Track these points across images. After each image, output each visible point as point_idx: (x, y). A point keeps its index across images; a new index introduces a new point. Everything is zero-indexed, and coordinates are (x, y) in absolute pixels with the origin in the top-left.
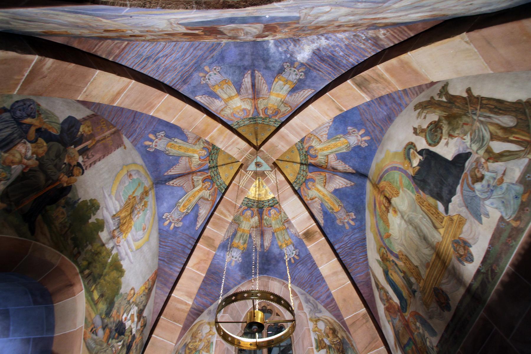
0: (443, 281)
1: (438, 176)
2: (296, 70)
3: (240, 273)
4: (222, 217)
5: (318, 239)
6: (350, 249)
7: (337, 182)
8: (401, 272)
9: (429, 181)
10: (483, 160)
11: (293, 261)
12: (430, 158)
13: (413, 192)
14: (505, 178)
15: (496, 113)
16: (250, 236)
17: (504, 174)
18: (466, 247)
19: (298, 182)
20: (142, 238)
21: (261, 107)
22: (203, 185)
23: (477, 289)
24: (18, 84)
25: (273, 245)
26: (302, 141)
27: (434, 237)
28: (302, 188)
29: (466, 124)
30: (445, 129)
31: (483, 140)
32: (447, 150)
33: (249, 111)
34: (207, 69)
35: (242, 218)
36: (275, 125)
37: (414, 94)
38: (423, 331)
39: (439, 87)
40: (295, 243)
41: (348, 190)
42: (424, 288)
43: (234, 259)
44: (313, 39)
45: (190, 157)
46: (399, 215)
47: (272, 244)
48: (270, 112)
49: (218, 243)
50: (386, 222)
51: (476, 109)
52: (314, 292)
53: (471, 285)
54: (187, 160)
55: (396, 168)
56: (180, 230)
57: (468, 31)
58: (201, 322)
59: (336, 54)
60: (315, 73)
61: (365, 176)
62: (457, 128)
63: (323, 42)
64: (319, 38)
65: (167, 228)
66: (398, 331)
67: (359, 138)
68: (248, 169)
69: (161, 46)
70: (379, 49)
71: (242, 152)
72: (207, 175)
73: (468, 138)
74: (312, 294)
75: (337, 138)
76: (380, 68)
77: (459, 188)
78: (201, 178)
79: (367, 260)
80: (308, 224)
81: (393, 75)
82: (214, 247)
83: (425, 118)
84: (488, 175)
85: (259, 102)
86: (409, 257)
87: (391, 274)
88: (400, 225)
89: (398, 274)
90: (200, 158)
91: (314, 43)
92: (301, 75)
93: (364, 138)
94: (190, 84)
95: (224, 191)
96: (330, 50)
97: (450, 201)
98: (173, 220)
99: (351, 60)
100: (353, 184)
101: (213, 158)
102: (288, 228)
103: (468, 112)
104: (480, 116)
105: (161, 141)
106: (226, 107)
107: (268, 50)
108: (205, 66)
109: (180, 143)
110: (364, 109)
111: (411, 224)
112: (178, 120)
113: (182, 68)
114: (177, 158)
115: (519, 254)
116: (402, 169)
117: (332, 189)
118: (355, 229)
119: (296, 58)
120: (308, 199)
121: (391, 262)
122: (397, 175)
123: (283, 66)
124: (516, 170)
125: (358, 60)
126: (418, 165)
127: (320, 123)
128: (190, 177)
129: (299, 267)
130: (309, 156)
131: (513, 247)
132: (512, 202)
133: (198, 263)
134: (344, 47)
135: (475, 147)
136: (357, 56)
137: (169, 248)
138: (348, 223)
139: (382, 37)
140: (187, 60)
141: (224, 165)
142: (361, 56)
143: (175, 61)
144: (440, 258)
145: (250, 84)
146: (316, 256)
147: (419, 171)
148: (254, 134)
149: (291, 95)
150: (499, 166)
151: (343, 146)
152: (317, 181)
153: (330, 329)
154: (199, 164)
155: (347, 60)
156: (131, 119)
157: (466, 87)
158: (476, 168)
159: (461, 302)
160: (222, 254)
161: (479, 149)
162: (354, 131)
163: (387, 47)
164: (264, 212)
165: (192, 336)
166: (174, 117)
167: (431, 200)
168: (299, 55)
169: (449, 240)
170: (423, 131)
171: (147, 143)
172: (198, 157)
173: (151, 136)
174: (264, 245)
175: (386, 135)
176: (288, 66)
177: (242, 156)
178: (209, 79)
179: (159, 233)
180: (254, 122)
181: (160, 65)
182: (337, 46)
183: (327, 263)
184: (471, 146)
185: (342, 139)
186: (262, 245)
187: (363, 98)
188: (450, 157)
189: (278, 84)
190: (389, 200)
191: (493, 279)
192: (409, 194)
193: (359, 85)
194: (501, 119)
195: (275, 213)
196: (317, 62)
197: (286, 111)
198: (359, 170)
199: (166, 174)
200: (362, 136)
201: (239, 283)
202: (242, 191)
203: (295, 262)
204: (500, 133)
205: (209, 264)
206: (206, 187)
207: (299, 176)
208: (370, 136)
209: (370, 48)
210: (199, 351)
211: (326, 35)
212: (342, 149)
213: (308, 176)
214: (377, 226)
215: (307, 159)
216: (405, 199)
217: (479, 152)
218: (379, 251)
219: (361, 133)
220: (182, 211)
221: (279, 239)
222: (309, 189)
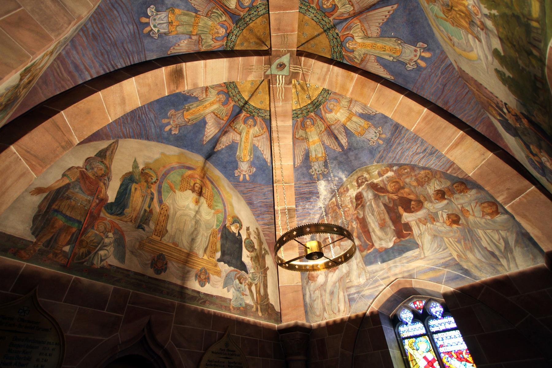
0: (174, 264)
6: (139, 117)
7: (212, 129)
8: (149, 207)
11: (144, 20)
13: (217, 226)
21: (319, 122)
24: (527, 194)
33: (326, 113)
34: (381, 142)
40: (167, 37)
41: (201, 136)
45: (367, 37)
48: (308, 122)
52: (85, 39)
53: (187, 288)
54: (369, 32)
59: (309, 203)
60: (307, 180)
63: (321, 204)
67: (244, 173)
69: (422, 163)
74: (81, 33)
77: (232, 268)
78: (341, 10)
80: (189, 81)
84: (243, 286)
85: (323, 126)
86: (170, 221)
88: (187, 207)
89: (144, 201)
90: (353, 38)
93: (242, 176)
94: (391, 125)
100: (205, 143)
101: (335, 40)
102: (191, 38)
105: (410, 57)
106: (349, 107)
107: (343, 171)
108: (383, 144)
109: (384, 54)
110: (263, 189)
111: (196, 222)
112: (395, 99)
113: (402, 141)
114: (383, 34)
115: (221, 314)
118: (161, 130)
121: (149, 192)
124: (249, 301)
128: (357, 8)
129: (131, 27)
130: (248, 115)
131: (222, 310)
134: (310, 211)
135: (250, 275)
138: (169, 124)
140: (399, 148)
143: (410, 147)
145: (340, 139)
149: (305, 150)
152: (222, 107)
154: (350, 29)
156: (447, 88)
159: (170, 283)
164: (230, 22)
166: (400, 104)
167: (219, 246)
171: (427, 55)
172: (356, 38)
173: (422, 64)
178: (375, 133)
181: (421, 145)
182: (313, 209)
183: (138, 91)
185: (248, 158)
191: (201, 303)
192: (214, 221)
195: (218, 33)
196: (312, 189)
198: (215, 155)
199: (395, 6)
200: (244, 175)
203: (141, 23)
208: (242, 182)
213: (231, 101)
218: (148, 166)
219: (247, 176)
221: (185, 15)
222: (218, 94)
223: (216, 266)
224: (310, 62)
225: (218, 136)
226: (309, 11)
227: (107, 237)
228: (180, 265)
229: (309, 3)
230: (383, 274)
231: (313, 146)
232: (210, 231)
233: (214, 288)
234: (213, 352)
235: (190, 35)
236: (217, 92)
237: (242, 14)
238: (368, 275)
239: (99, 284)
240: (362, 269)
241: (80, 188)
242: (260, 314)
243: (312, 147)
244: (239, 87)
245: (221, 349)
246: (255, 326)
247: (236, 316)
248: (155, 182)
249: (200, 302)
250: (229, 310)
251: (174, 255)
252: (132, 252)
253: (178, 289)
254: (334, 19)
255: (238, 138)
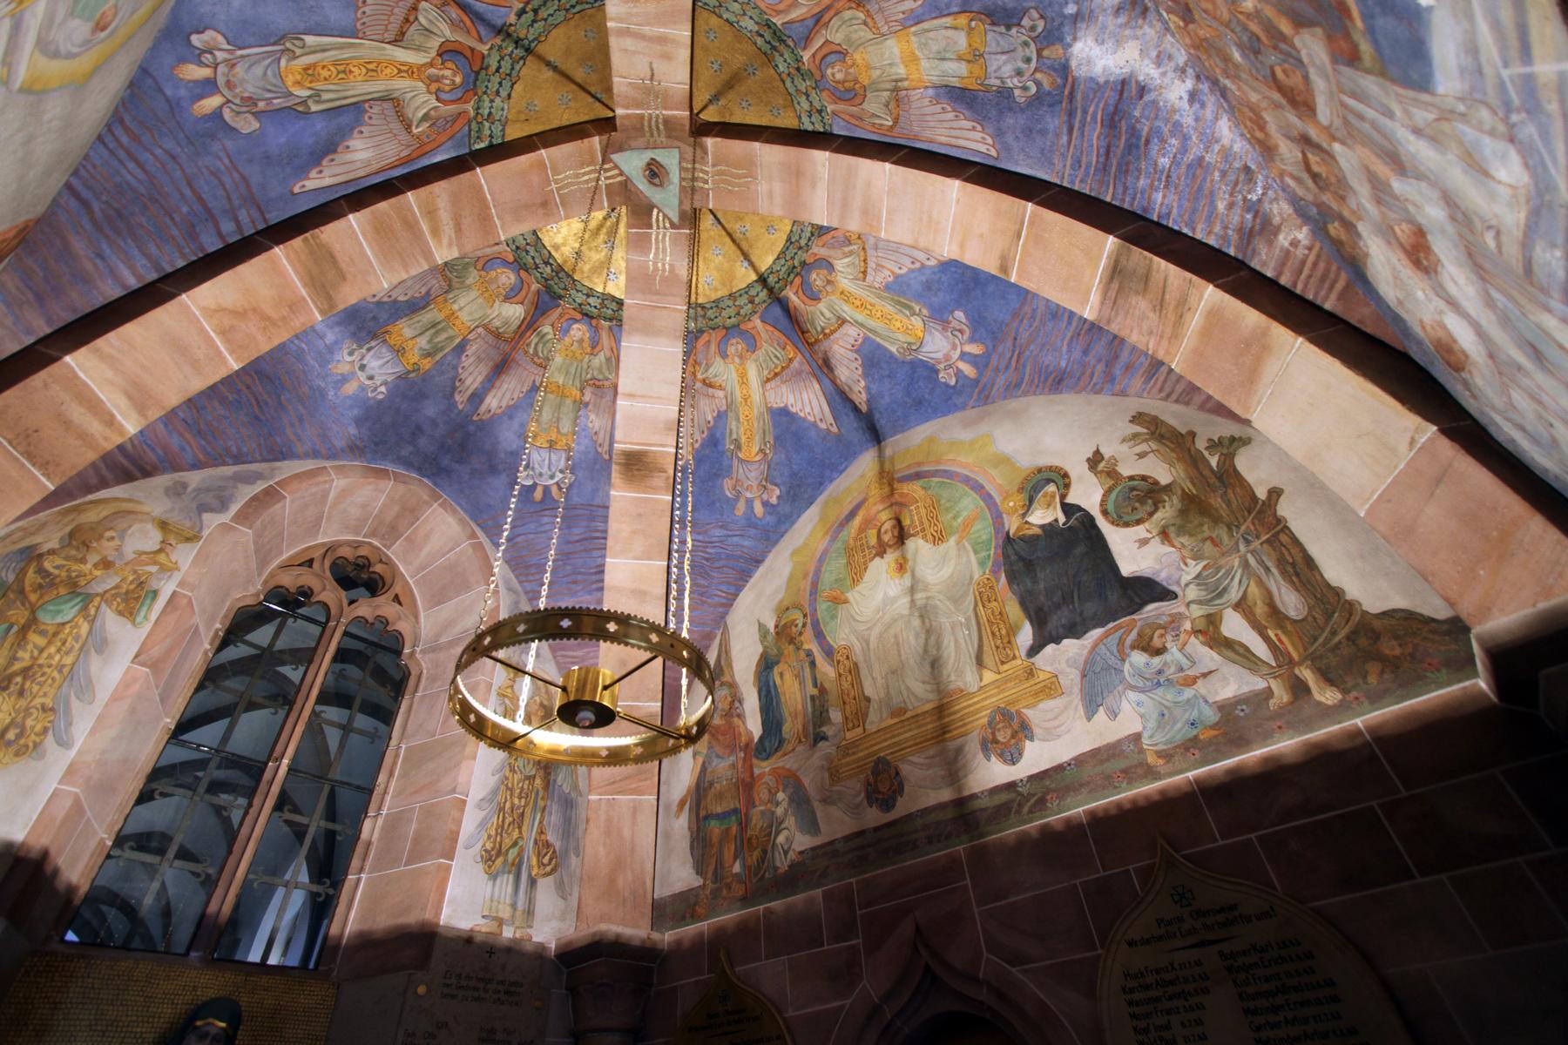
0: (915, 759)
1: (1064, 579)
2: (1033, 65)
3: (353, 430)
4: (425, 227)
5: (655, 490)
7: (805, 396)
8: (815, 685)
9: (1041, 575)
10: (1187, 626)
11: (538, 494)
12: (1081, 534)
13: (982, 564)
14: (1200, 682)
15: (1284, 573)
16: (461, 348)
17: (1205, 675)
18: (1020, 735)
19: (710, 313)
20: (70, 56)
21: (836, 33)
22: (431, 64)
23: (985, 809)
25: (511, 417)
26: (820, 231)
27: (960, 673)
28: (705, 337)
29: (1215, 543)
30: (1165, 514)
31: (1220, 595)
32: (1134, 551)
35: (473, 277)
36: (805, 119)
37: (1161, 390)
38: (786, 814)
39: (1227, 429)
41: (813, 433)
42: (854, 744)
43: (362, 376)
44: (1170, 57)
46: (907, 580)
47: (510, 412)
48: (836, 73)
49: (349, 296)
50: (856, 574)
51: (1258, 537)
53: (973, 797)
55: (978, 488)
56: (229, 144)
57: (1443, 431)
58: (129, 506)
60: (1054, 122)
61: (875, 435)
62: (1191, 535)
63: (1176, 92)
64: (1183, 71)
65: (183, 92)
66: (711, 784)
68: (615, 157)
70: (1237, 248)
71: (650, 91)
72: (471, 42)
73: (1194, 568)
75: (909, 308)
76: (1210, 295)
77: (1096, 633)
79: (728, 605)
81: (1206, 332)
82: (329, 298)
83: (1141, 456)
84: (1174, 654)
85: (847, 14)
86: (864, 672)
87: (781, 675)
88: (889, 601)
89: (802, 684)
91: (1158, 64)
92: (1025, 88)
95: (482, 145)
96: (1158, 123)
97: (1057, 640)
98: (229, 85)
99: (1158, 197)
101: (543, 13)
102: (587, 405)
103: (1238, 527)
104: (1252, 552)
110: (1034, 311)
111: (921, 616)
115: (1118, 805)
116: (995, 504)
117: (777, 403)
119: (1075, 39)
120: (699, 376)
121: (802, 654)
122: (969, 503)
123: (1025, 12)
124: (1232, 684)
125: (1169, 214)
126: (1042, 527)
127: (922, 243)
130: (798, 281)
131: (1117, 790)
132: (1179, 725)
133: (241, 314)
135: (1193, 593)
136: (1180, 206)
137: (141, 176)
138: (749, 502)
139: (1283, 240)
141: (555, 69)
142: (1186, 217)
144: (941, 718)
146: (618, 526)
147: (1035, 538)
148: (725, 76)
149: (936, 100)
150: (1209, 658)
151: (901, 337)
152: (760, 353)
153: (542, 705)
155: (1152, 186)
157: (1275, 483)
158: (1164, 628)
159: (925, 812)
160: (330, 337)
161: (1200, 602)
162: (961, 331)
163: (1255, 264)
164: (555, 314)
165: (71, 535)
167: (1014, 610)
168: (1090, 42)
169: (995, 700)
170: (1112, 474)
174: (482, 401)
175: (1013, 404)
176: (1033, 28)
177: (638, 105)
179: (133, 85)
180: (766, 48)
182: (1185, 138)
184: (1187, 585)
185: (917, 322)
186: (477, 398)
187: (1085, 301)
188: (1126, 569)
189: (950, 33)
190: (901, 536)
191: (1031, 812)
192: (969, 562)
193: (1116, 271)
194: (1283, 590)
195: (581, 341)
196: (1097, 110)
197: (875, 118)
198: (877, 416)
200: (964, 356)
201: (333, 455)
202: (544, 204)
204: (1260, 610)
205: (276, 342)
206: (438, 79)
207: (730, 303)
208: (980, 374)
209: (1226, 228)
210: (88, 598)
211: (1205, 87)
212: (894, 341)
213: (750, 325)
214: (821, 561)
215: (786, 283)
216: (950, 565)
217: (1193, 607)
218: (782, 610)
219: (969, 348)
220: (290, 81)
222: (724, 356)
223: (1030, 673)
224: (624, 89)
225: (830, 387)
226: (490, 114)
227: (778, 804)
228: (932, 752)
229: (470, 122)
230: (1496, 26)
231: (924, 64)
232: (969, 601)
233: (1061, 737)
234: (1131, 944)
235: (581, 405)
236: (718, 359)
237: (535, 286)
238: (1484, 114)
239: (798, 899)
240: (1445, 126)
241: (718, 756)
242: (1328, 696)
243: (931, 71)
244: (720, 294)
245: (1160, 922)
246: (1321, 760)
247: (1191, 775)
248: (804, 625)
249: (1026, 809)
250: (1151, 773)
251: (907, 740)
252: (825, 801)
253: (950, 814)
254: (481, 40)
255: (851, 333)
